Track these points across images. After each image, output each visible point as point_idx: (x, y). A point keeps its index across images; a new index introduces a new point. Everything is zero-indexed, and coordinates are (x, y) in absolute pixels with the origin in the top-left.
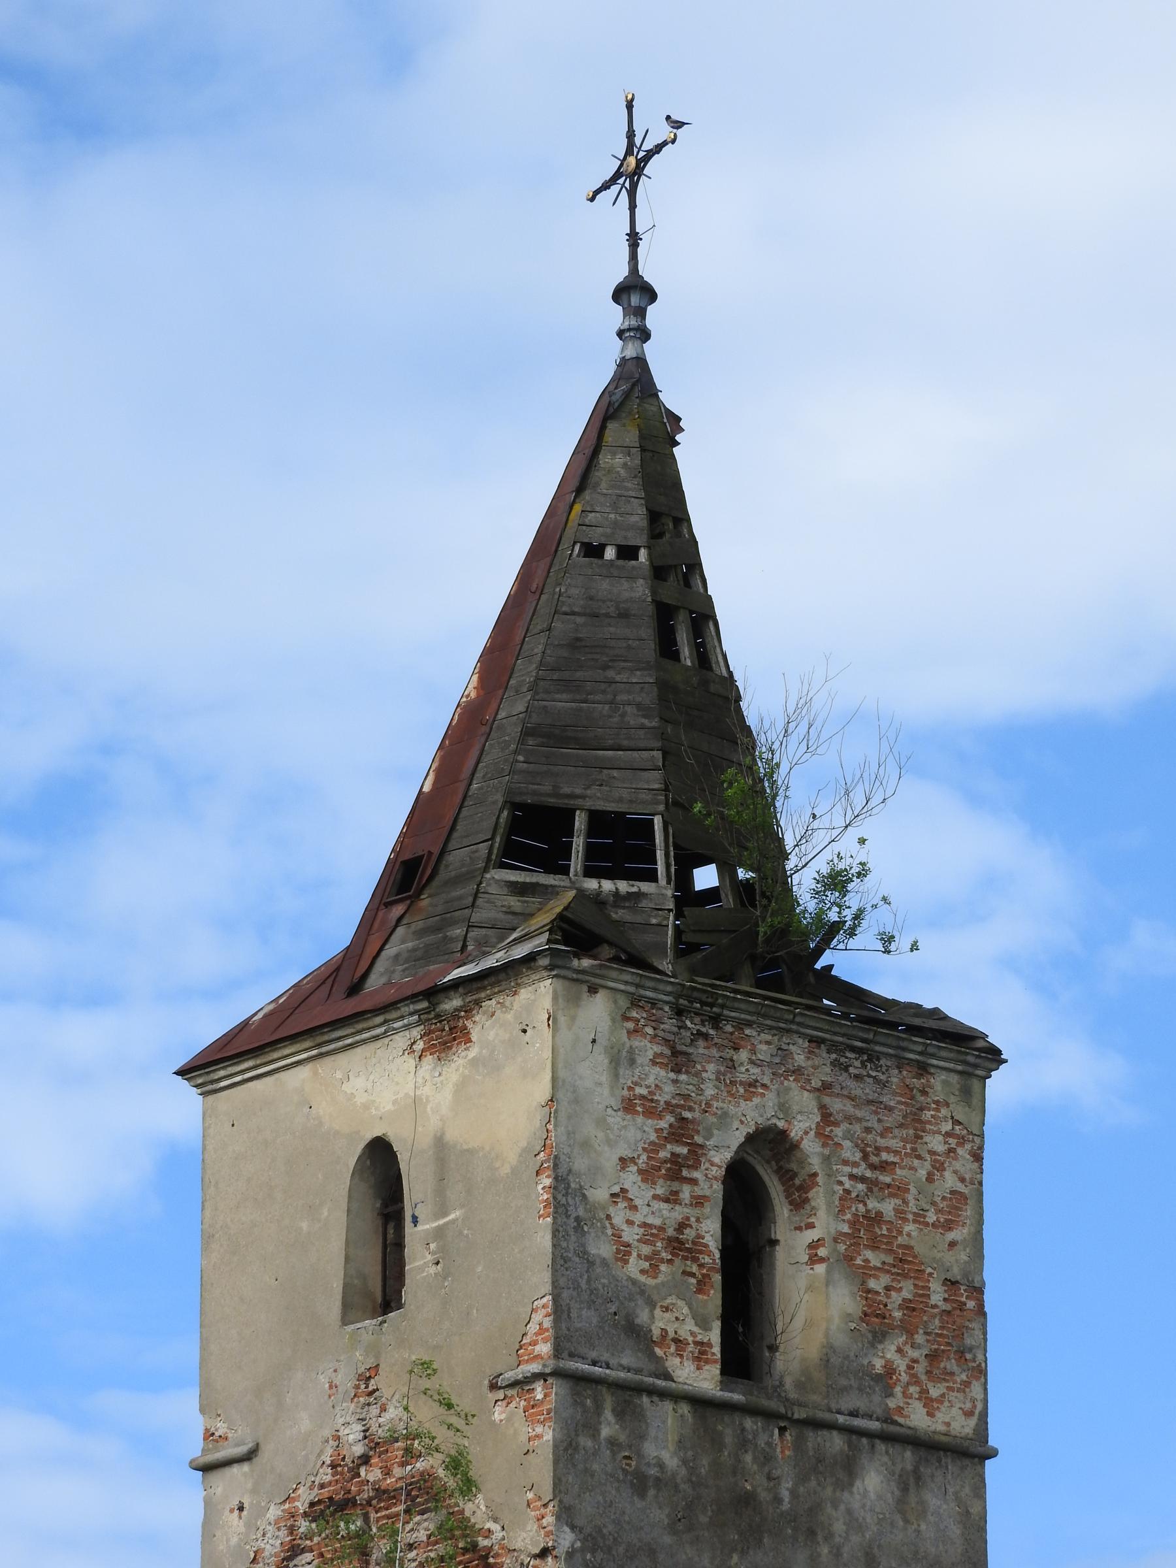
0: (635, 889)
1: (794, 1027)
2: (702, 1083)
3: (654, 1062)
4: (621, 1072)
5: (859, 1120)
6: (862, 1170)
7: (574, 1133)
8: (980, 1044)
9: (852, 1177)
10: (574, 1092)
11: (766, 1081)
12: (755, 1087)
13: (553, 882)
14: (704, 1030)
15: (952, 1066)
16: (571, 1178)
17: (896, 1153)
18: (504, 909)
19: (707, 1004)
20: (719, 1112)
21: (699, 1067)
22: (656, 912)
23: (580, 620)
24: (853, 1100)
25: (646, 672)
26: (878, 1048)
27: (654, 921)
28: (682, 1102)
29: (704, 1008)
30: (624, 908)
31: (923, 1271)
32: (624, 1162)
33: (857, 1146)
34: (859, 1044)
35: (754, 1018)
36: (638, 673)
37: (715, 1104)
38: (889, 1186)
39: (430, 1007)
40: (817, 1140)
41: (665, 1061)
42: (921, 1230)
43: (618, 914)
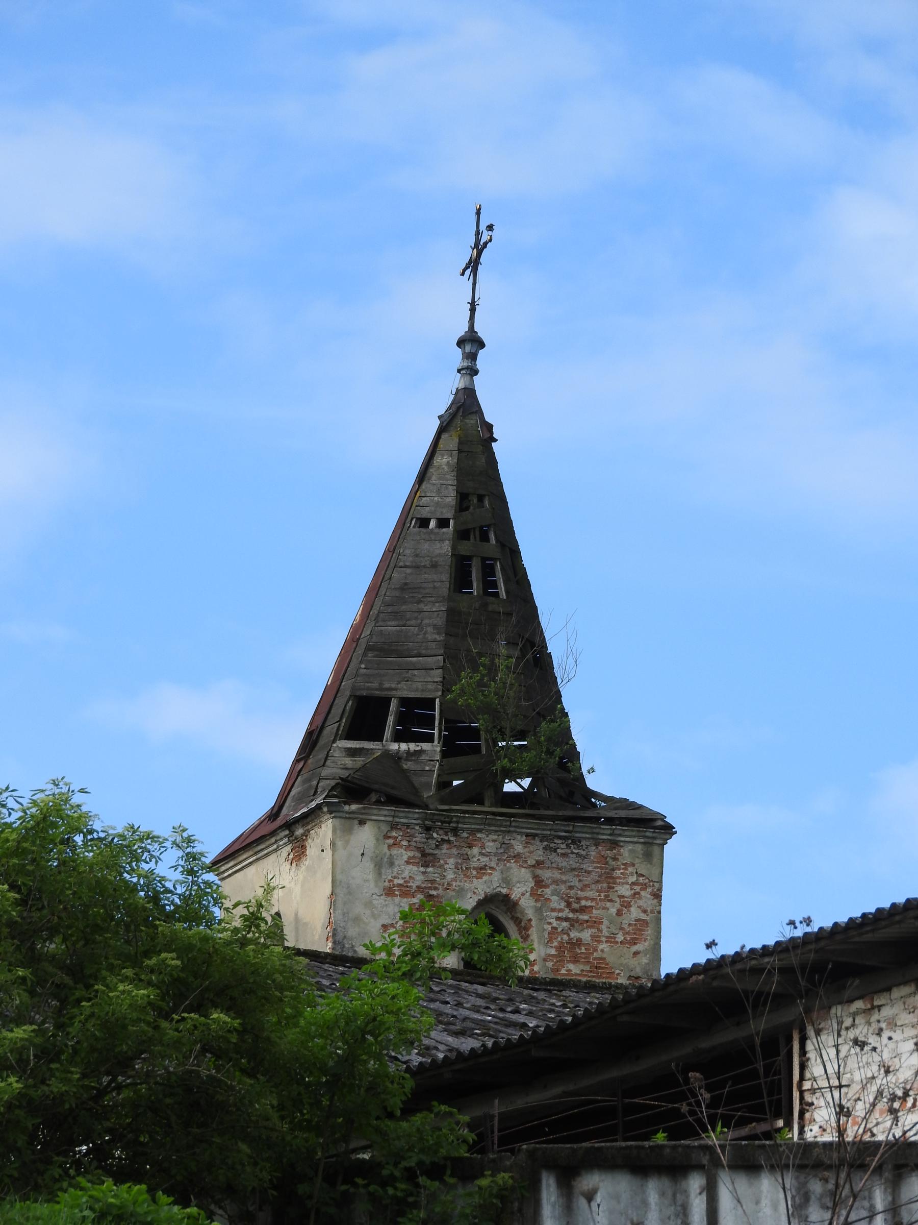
0: (419, 748)
1: (512, 829)
2: (445, 872)
3: (408, 862)
4: (383, 871)
5: (565, 882)
6: (567, 913)
7: (348, 913)
8: (659, 823)
9: (558, 919)
10: (348, 887)
11: (493, 864)
12: (486, 869)
13: (372, 747)
14: (446, 838)
15: (636, 840)
16: (345, 941)
17: (593, 900)
18: (341, 766)
19: (446, 822)
20: (457, 889)
21: (442, 862)
22: (429, 762)
23: (408, 571)
24: (560, 870)
25: (441, 604)
26: (577, 835)
27: (427, 768)
28: (430, 885)
29: (444, 824)
30: (411, 761)
31: (614, 972)
32: (385, 927)
33: (562, 898)
34: (564, 834)
35: (482, 827)
36: (437, 604)
37: (454, 884)
38: (587, 921)
39: (289, 834)
40: (531, 898)
41: (417, 860)
42: (612, 946)
43: (408, 765)
